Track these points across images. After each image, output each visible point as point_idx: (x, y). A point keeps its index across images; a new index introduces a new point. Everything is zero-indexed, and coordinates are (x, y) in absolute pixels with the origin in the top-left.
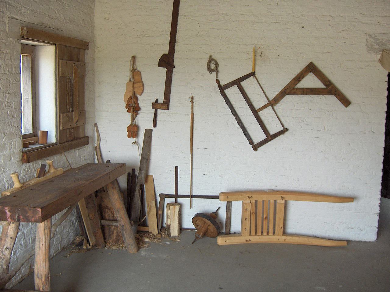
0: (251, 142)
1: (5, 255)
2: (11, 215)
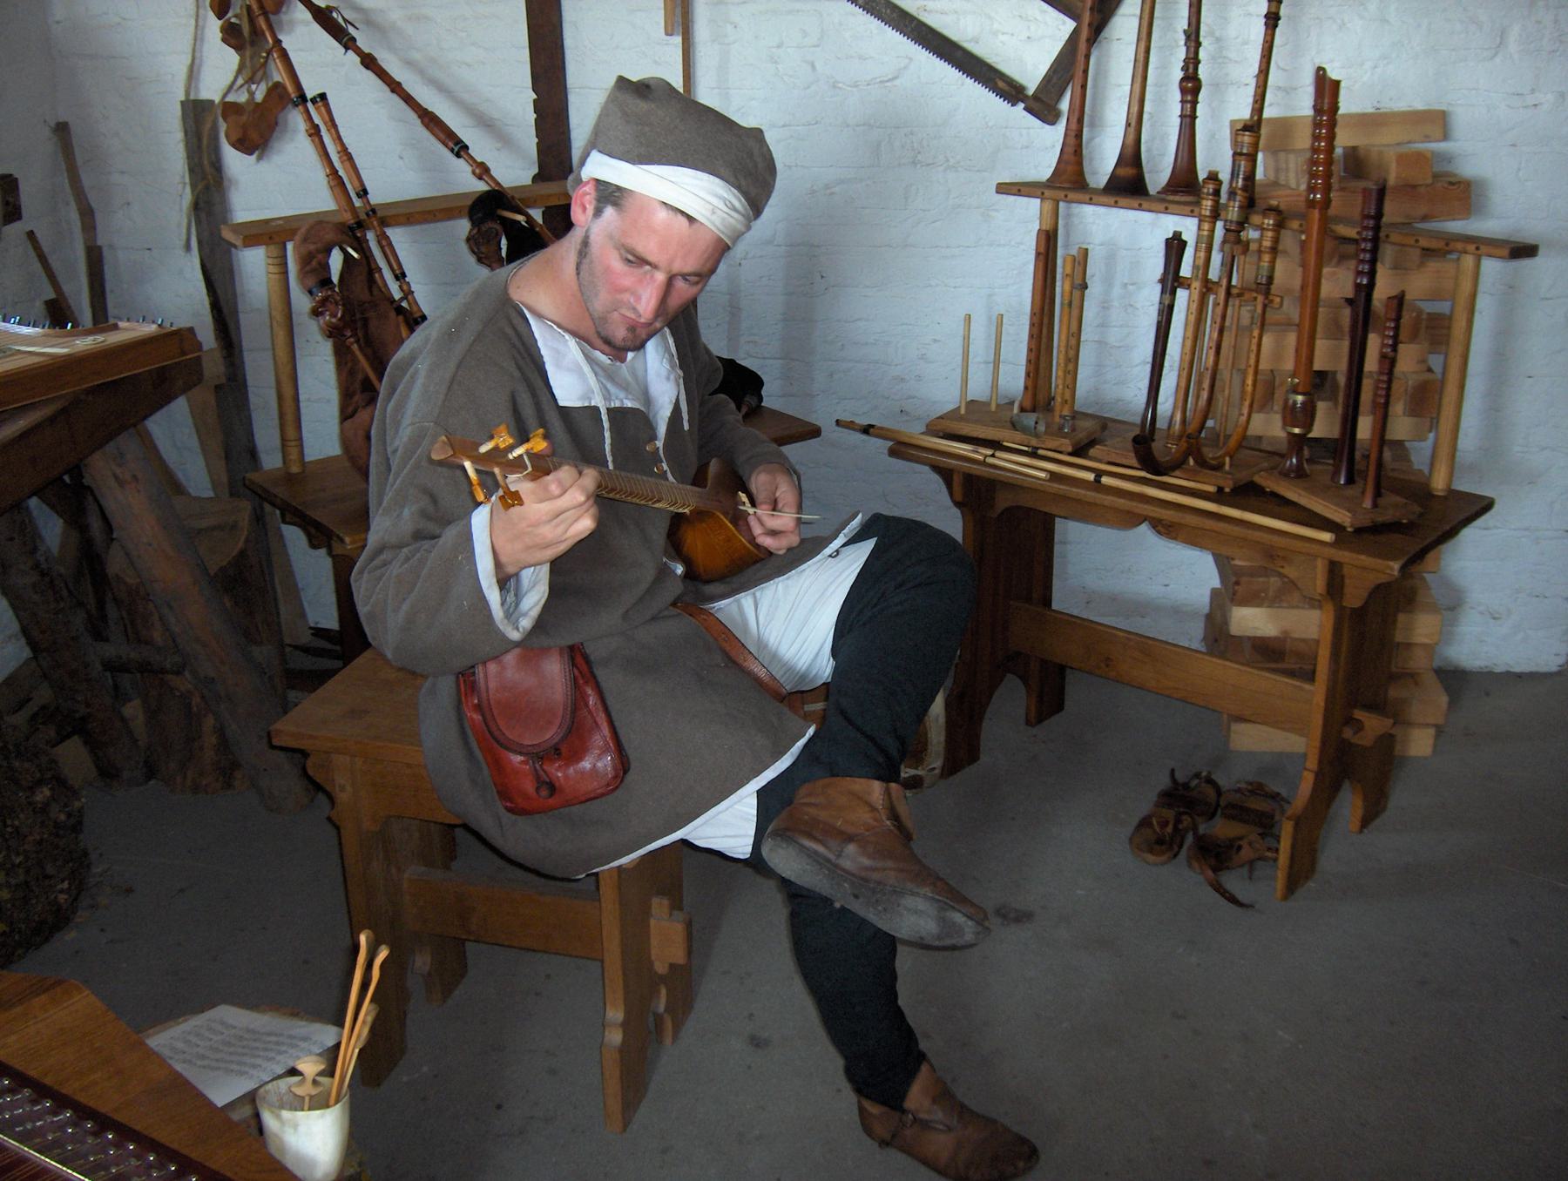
0: (1010, 91)
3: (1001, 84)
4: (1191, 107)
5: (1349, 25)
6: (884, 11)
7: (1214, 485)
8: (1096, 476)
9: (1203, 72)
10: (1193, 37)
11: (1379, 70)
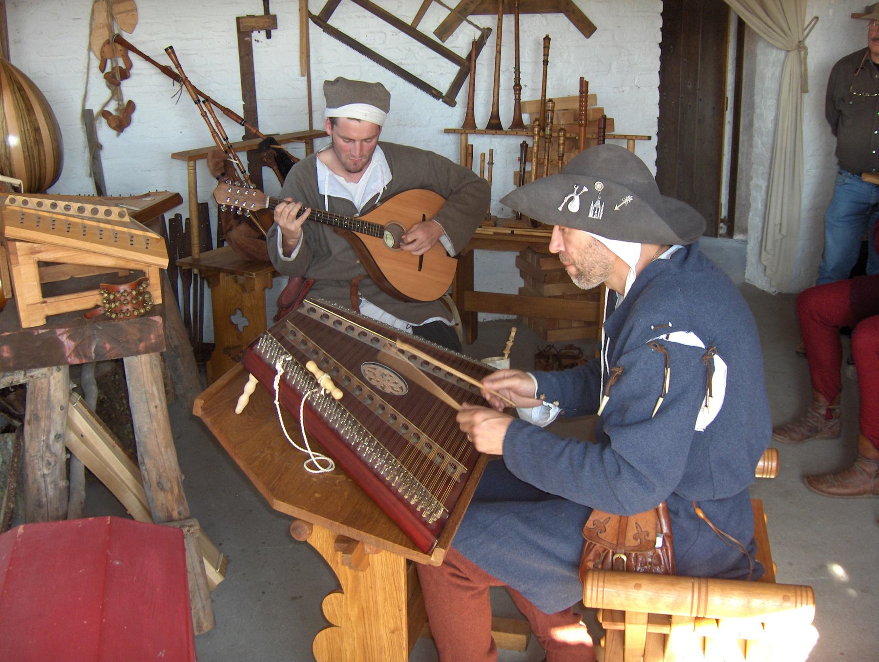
0: (435, 94)
1: (56, 456)
2: (76, 347)
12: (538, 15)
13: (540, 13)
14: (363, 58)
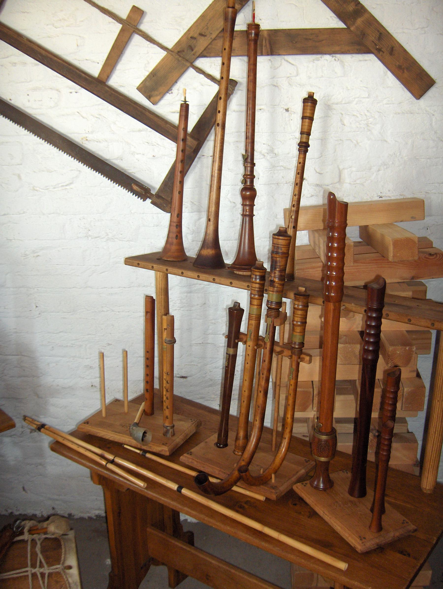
3: (135, 187)
4: (249, 209)
5: (360, 144)
6: (58, 142)
7: (264, 496)
8: (178, 487)
9: (257, 185)
10: (249, 160)
11: (381, 172)
12: (327, 57)
13: (330, 54)
14: (226, 139)
